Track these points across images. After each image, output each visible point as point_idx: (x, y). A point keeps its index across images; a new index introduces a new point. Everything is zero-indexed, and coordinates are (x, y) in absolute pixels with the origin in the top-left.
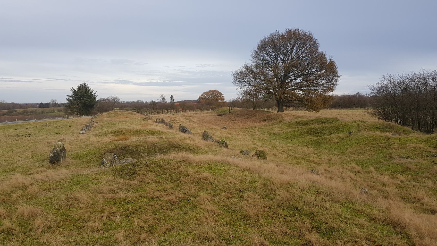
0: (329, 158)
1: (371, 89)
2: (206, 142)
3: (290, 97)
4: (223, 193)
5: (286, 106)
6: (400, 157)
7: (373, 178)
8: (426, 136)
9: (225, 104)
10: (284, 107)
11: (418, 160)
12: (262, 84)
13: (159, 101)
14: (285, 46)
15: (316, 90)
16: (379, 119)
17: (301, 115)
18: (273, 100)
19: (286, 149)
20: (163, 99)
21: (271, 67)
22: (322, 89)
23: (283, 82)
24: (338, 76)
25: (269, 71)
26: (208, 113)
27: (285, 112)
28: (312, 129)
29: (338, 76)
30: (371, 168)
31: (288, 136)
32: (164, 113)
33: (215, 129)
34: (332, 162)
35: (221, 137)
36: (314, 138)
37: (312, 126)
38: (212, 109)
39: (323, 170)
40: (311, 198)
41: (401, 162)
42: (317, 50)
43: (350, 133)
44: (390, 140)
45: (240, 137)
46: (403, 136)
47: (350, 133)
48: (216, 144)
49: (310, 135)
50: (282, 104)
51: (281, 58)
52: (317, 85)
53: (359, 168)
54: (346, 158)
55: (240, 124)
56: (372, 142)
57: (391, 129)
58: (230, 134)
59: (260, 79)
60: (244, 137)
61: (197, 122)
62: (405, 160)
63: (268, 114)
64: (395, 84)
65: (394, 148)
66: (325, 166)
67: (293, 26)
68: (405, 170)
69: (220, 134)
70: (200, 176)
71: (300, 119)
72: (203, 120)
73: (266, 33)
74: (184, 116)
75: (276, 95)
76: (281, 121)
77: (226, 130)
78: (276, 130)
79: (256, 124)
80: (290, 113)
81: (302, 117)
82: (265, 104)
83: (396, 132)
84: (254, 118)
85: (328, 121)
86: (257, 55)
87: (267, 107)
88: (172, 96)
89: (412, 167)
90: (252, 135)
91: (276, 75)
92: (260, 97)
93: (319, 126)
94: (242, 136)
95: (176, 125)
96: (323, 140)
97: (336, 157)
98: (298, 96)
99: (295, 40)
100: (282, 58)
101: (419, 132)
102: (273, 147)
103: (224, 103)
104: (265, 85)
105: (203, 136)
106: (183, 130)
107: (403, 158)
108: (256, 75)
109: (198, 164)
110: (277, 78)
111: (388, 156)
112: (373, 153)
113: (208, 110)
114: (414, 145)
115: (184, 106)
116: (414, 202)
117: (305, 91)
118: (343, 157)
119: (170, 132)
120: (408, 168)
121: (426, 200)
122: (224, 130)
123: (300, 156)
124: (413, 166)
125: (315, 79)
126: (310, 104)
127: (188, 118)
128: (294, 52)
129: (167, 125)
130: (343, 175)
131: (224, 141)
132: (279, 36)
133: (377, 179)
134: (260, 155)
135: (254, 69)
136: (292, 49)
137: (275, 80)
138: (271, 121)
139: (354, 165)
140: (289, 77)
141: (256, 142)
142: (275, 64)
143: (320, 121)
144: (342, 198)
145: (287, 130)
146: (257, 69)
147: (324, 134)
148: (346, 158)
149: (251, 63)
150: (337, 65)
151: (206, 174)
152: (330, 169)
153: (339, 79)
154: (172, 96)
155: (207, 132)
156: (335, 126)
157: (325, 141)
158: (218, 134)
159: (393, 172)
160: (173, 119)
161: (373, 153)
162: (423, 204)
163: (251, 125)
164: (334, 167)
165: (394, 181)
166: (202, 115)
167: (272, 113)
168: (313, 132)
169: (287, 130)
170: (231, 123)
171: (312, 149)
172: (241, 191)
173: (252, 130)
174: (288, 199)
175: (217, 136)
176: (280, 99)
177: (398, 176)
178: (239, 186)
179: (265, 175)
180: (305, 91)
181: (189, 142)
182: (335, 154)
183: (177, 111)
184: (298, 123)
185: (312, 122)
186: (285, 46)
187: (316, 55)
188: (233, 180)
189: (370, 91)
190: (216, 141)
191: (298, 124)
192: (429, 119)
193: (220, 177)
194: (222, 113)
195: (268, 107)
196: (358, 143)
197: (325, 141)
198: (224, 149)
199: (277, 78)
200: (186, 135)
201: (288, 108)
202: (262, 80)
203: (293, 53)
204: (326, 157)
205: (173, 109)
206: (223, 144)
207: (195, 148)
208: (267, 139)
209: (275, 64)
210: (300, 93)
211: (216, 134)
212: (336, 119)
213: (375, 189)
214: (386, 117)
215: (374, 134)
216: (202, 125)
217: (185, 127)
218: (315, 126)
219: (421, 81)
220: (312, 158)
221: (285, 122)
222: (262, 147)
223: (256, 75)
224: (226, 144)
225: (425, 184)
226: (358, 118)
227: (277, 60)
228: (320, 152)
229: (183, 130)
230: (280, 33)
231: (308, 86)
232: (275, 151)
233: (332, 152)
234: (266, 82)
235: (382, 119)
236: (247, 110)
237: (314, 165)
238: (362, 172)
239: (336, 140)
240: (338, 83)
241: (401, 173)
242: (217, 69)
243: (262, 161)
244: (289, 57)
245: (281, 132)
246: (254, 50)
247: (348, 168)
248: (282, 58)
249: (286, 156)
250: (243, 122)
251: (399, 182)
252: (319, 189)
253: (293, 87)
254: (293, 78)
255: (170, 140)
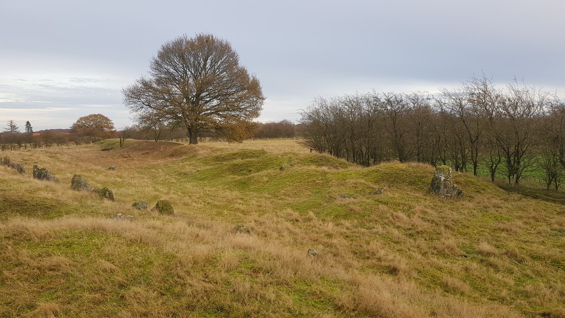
0: (259, 204)
1: (301, 114)
2: (77, 192)
3: (205, 124)
4: (87, 294)
5: (201, 136)
6: (341, 196)
7: (315, 226)
8: (366, 170)
9: (114, 134)
10: (198, 138)
11: (361, 199)
12: (167, 106)
13: (6, 130)
14: (196, 57)
15: (238, 115)
16: (311, 150)
17: (221, 147)
18: (183, 127)
19: (202, 194)
20: (13, 127)
21: (178, 84)
22: (245, 114)
23: (196, 103)
24: (263, 99)
25: (175, 89)
26: (87, 147)
27: (199, 144)
28: (235, 165)
29: (263, 99)
30: (311, 214)
31: (204, 177)
32: (13, 148)
33: (96, 171)
34: (262, 208)
35: (105, 183)
36: (238, 178)
37: (235, 162)
38: (93, 142)
39: (253, 222)
40: (244, 284)
41: (343, 203)
42: (236, 64)
43: (281, 169)
44: (328, 176)
45: (136, 181)
46: (341, 170)
47: (281, 169)
48: (93, 195)
49: (233, 173)
50: (195, 133)
51: (191, 72)
52: (239, 109)
53: (296, 215)
54: (278, 201)
55: (136, 162)
56: (308, 178)
57: (326, 162)
58: (120, 177)
59: (164, 98)
60: (141, 181)
61: (69, 161)
62: (347, 200)
63: (176, 148)
64: (327, 108)
65: (332, 186)
66: (255, 216)
67: (205, 31)
68: (349, 214)
69: (104, 178)
70: (47, 262)
71: (219, 153)
72: (77, 158)
73: (170, 37)
74: (47, 152)
75: (186, 121)
76: (194, 156)
77: (114, 172)
78: (188, 169)
79: (159, 161)
80: (207, 146)
81: (221, 150)
82: (172, 132)
83: (332, 166)
84: (156, 152)
85: (253, 154)
86: (157, 66)
87: (175, 138)
88: (28, 123)
89: (357, 208)
90: (154, 178)
91: (186, 95)
92: (166, 123)
93: (243, 161)
94: (137, 181)
95: (28, 168)
96: (249, 179)
97: (267, 202)
98: (216, 122)
99: (208, 49)
100: (193, 72)
101: (355, 164)
102: (184, 193)
103: (112, 132)
104: (171, 107)
105: (73, 183)
106: (40, 174)
107: (344, 197)
108: (157, 94)
109: (43, 238)
110: (187, 98)
111: (327, 195)
112: (309, 193)
113: (88, 143)
114: (354, 181)
115: (49, 138)
116: (368, 258)
117: (225, 117)
118: (275, 200)
119: (13, 180)
120: (351, 210)
121: (382, 253)
122: (111, 171)
123: (221, 203)
124: (358, 207)
125: (236, 101)
126: (230, 132)
127: (53, 156)
128: (208, 66)
129: (13, 167)
130: (279, 226)
131: (107, 190)
132: (187, 42)
133: (319, 228)
134: (164, 208)
135: (155, 85)
136: (206, 60)
137: (185, 100)
138: (181, 156)
139: (289, 210)
140: (203, 98)
141: (159, 187)
142: (184, 79)
143: (244, 154)
144: (289, 275)
145: (202, 168)
146: (158, 85)
147: (250, 171)
148: (278, 201)
149: (149, 76)
150: (261, 84)
151: (59, 258)
152: (261, 219)
153: (264, 101)
154: (28, 123)
155: (79, 176)
156: (263, 161)
157: (252, 181)
158: (101, 177)
159: (336, 217)
160: (26, 158)
161: (309, 193)
162: (379, 259)
163: (152, 163)
164: (267, 215)
165: (339, 229)
166: (77, 150)
167: (182, 146)
168: (235, 169)
169: (202, 168)
170: (123, 161)
171: (236, 192)
172: (121, 286)
173: (154, 170)
174: (206, 291)
175: (98, 182)
176: (192, 126)
177: (343, 221)
178: (119, 278)
179: (168, 248)
180: (225, 117)
181: (44, 194)
182: (265, 197)
183: (36, 146)
184: (217, 158)
185: (234, 156)
186: (196, 57)
187: (236, 71)
188: (108, 265)
189: (301, 117)
190: (94, 191)
191: (217, 159)
192: (364, 149)
193: (85, 261)
194: (110, 147)
195: (177, 138)
196: (292, 182)
197: (252, 181)
198: (107, 203)
199: (187, 98)
200: (41, 183)
201: (203, 139)
202: (167, 100)
203: (207, 66)
204: (254, 202)
205: (30, 142)
206: (105, 194)
207: (54, 204)
208: (175, 181)
209: (184, 79)
210: (217, 118)
211: (97, 179)
212: (263, 152)
213: (320, 243)
214: (320, 149)
215: (309, 168)
216: (76, 165)
217: (44, 169)
218: (238, 161)
219: (355, 105)
220: (237, 206)
221: (199, 157)
222: (168, 193)
223: (157, 94)
224: (110, 194)
225: (375, 230)
226: (287, 150)
227: (187, 75)
228: (247, 195)
229: (40, 174)
230: (189, 38)
231: (228, 109)
232: (187, 199)
233: (262, 195)
234: (172, 103)
235: (317, 150)
236: (146, 142)
237: (240, 215)
238: (300, 220)
239: (265, 179)
240: (263, 107)
241: (346, 217)
242: (108, 88)
243: (167, 218)
244: (202, 70)
245: (194, 171)
246: (154, 59)
247: (283, 216)
248: (193, 72)
249: (202, 205)
250: (141, 158)
251: (345, 230)
252: (254, 261)
253: (209, 111)
254: (208, 99)
255: (7, 194)
